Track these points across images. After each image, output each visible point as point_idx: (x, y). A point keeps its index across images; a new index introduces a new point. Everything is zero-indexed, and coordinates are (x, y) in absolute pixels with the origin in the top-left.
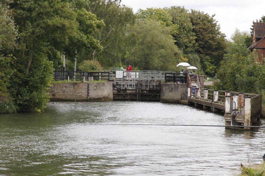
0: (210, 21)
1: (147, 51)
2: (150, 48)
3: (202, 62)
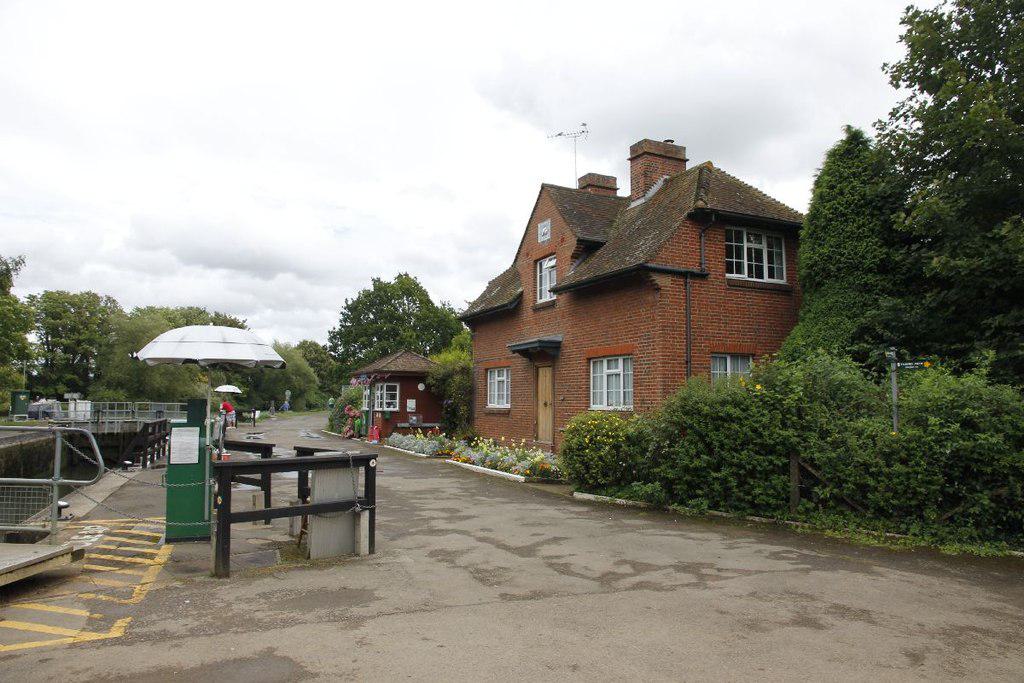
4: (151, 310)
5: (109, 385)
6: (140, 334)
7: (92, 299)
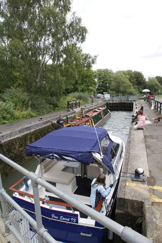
0: (141, 74)
3: (138, 88)
5: (111, 90)
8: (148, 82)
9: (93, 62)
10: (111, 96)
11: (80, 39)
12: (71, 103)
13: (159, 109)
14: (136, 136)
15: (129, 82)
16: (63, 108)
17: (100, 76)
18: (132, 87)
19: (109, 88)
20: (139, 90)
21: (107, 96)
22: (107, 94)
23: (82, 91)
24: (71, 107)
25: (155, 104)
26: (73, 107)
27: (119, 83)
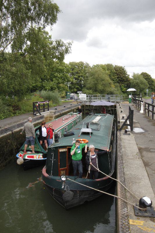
0: (123, 69)
1: (96, 82)
2: (97, 80)
3: (120, 87)
4: (98, 66)
5: (87, 89)
6: (95, 73)
7: (81, 64)
8: (131, 79)
9: (67, 51)
10: (87, 96)
11: (49, 20)
12: (38, 105)
13: (151, 114)
14: (128, 149)
15: (110, 80)
16: (26, 112)
17: (72, 70)
18: (113, 86)
19: (85, 86)
20: (121, 89)
21: (82, 96)
22: (82, 94)
23: (52, 89)
24: (38, 110)
25: (145, 106)
26: (40, 110)
27: (98, 80)
